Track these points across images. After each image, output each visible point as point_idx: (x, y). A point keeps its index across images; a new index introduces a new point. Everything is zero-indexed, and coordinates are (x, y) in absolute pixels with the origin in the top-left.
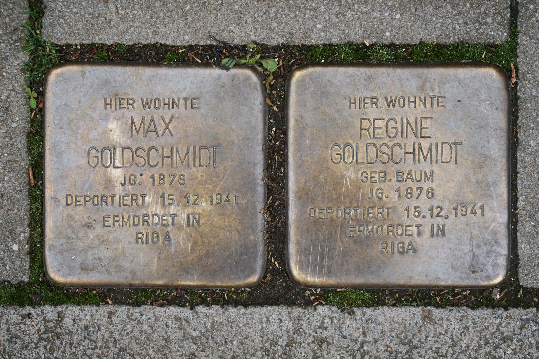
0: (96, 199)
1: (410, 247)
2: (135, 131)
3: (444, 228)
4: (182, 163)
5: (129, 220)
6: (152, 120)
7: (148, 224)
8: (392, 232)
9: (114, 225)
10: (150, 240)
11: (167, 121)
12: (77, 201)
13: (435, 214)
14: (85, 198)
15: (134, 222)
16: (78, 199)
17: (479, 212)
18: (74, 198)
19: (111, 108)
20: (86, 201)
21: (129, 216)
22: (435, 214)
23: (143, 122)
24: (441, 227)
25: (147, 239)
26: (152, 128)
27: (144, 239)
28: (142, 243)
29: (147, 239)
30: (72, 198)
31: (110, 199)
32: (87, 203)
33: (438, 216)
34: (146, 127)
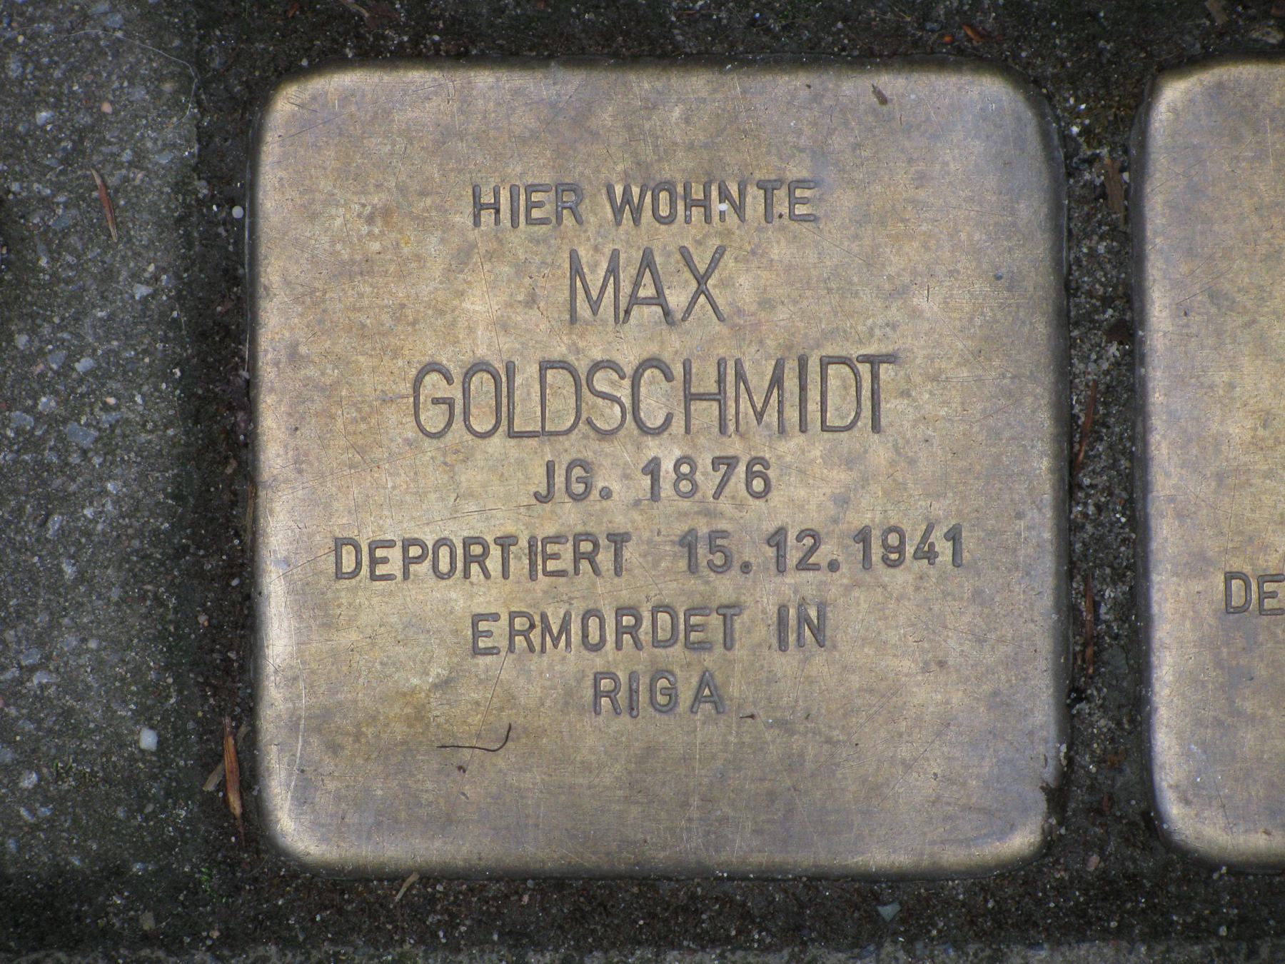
0: (444, 552)
1: (707, 692)
2: (587, 305)
3: (821, 615)
4: (759, 416)
5: (565, 627)
6: (647, 262)
7: (637, 644)
8: (525, 634)
9: (511, 648)
10: (643, 697)
11: (702, 268)
12: (374, 562)
13: (793, 557)
14: (405, 550)
15: (585, 636)
16: (379, 553)
17: (944, 549)
18: (1254, 587)
19: (497, 222)
20: (408, 561)
21: (567, 615)
22: (793, 557)
23: (613, 270)
24: (813, 613)
25: (633, 692)
26: (647, 291)
27: (622, 696)
28: (616, 711)
29: (633, 692)
30: (358, 550)
31: (495, 552)
32: (413, 568)
33: (803, 565)
34: (626, 288)
